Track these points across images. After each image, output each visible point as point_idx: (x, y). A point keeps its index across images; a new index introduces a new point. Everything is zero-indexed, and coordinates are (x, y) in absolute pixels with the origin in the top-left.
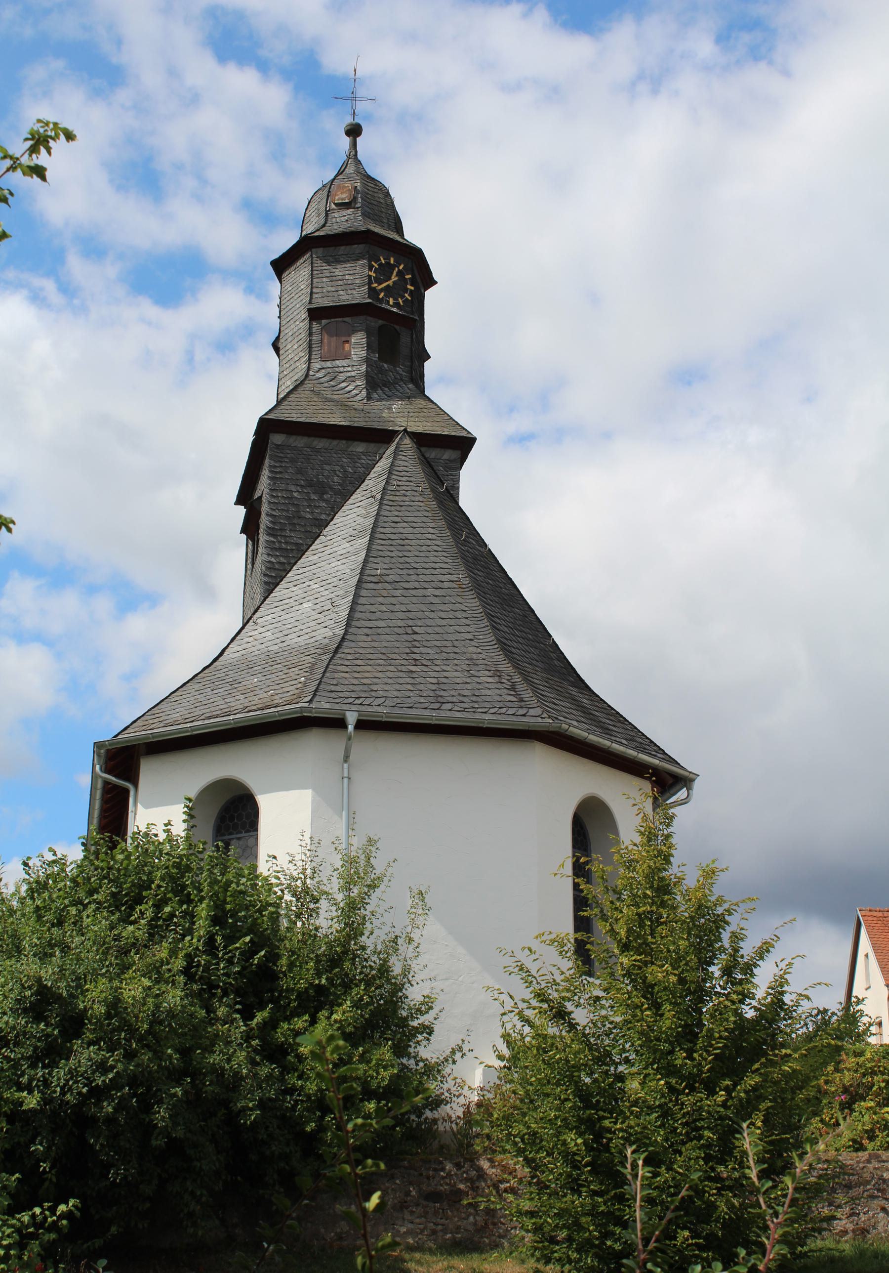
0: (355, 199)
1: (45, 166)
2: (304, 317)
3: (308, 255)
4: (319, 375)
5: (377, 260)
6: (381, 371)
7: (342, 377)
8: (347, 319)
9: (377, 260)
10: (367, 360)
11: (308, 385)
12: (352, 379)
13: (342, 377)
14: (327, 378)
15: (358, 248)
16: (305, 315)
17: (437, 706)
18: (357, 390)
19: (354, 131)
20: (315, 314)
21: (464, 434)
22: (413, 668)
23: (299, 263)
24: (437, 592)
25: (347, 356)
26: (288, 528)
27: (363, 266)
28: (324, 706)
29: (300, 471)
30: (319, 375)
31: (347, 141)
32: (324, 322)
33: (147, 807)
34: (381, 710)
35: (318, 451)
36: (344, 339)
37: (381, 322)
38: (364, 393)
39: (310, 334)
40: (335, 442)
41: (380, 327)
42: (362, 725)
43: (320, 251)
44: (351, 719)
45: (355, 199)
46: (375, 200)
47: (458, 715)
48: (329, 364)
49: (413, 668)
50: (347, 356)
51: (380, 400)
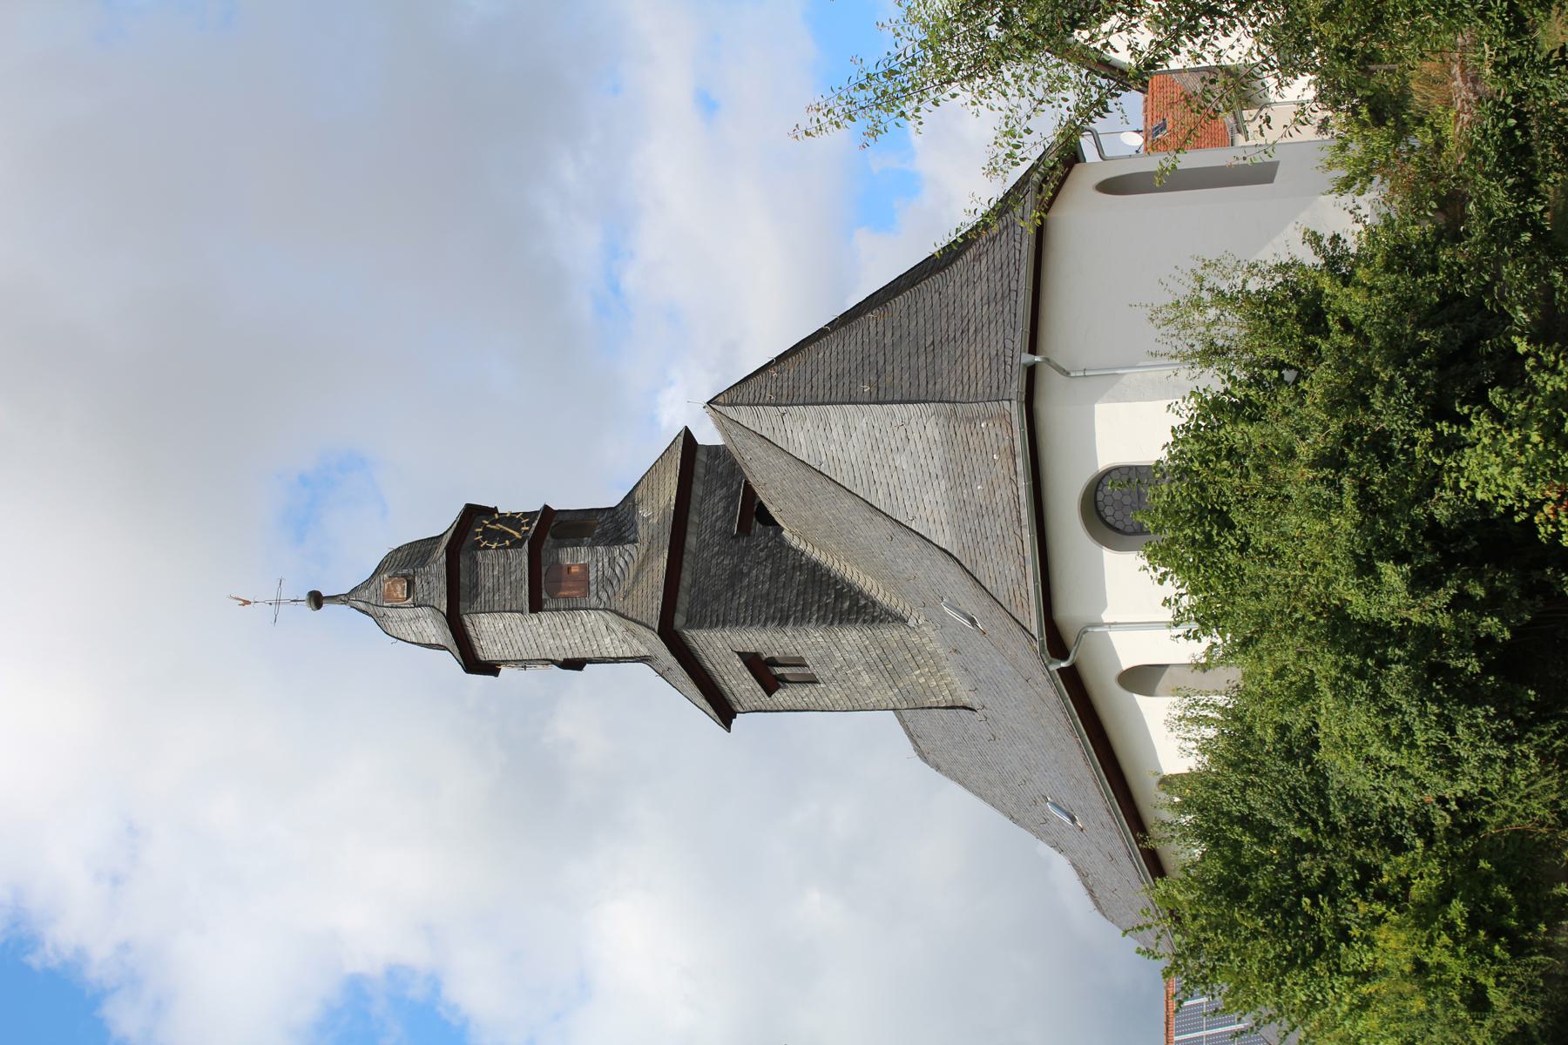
0: (404, 576)
1: (462, 506)
2: (536, 621)
3: (466, 618)
4: (605, 598)
5: (479, 542)
6: (604, 534)
7: (608, 572)
8: (544, 570)
9: (479, 542)
10: (592, 546)
11: (618, 604)
12: (612, 561)
13: (608, 572)
14: (610, 590)
15: (464, 562)
16: (534, 619)
17: (1013, 294)
18: (626, 556)
19: (317, 600)
20: (536, 606)
21: (681, 439)
22: (972, 331)
23: (472, 634)
24: (889, 334)
25: (585, 568)
26: (779, 605)
27: (484, 556)
28: (1017, 386)
29: (717, 598)
30: (605, 598)
31: (326, 607)
32: (544, 596)
33: (1103, 605)
34: (1021, 337)
35: (694, 582)
36: (565, 573)
37: (548, 537)
38: (627, 547)
39: (558, 610)
40: (685, 565)
41: (553, 536)
42: (1033, 350)
43: (462, 605)
44: (1027, 358)
45: (404, 576)
46: (406, 562)
47: (1023, 272)
48: (593, 588)
49: (972, 331)
50: (585, 568)
51: (636, 532)
